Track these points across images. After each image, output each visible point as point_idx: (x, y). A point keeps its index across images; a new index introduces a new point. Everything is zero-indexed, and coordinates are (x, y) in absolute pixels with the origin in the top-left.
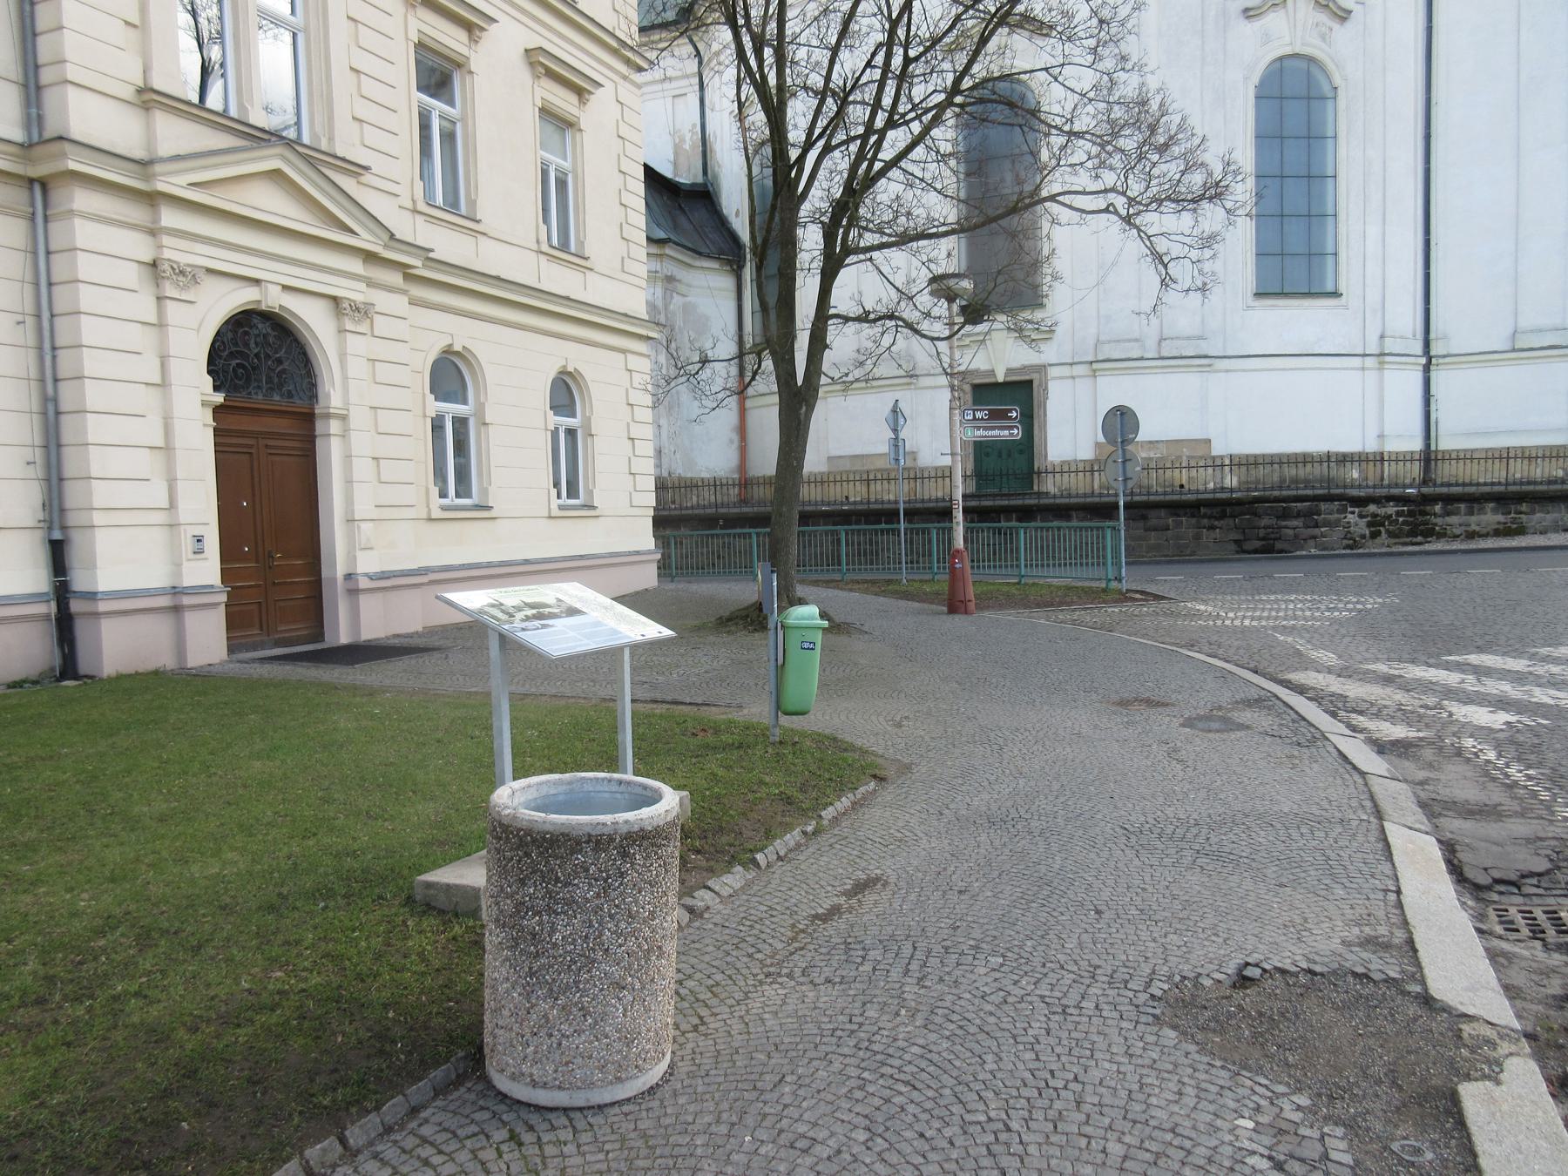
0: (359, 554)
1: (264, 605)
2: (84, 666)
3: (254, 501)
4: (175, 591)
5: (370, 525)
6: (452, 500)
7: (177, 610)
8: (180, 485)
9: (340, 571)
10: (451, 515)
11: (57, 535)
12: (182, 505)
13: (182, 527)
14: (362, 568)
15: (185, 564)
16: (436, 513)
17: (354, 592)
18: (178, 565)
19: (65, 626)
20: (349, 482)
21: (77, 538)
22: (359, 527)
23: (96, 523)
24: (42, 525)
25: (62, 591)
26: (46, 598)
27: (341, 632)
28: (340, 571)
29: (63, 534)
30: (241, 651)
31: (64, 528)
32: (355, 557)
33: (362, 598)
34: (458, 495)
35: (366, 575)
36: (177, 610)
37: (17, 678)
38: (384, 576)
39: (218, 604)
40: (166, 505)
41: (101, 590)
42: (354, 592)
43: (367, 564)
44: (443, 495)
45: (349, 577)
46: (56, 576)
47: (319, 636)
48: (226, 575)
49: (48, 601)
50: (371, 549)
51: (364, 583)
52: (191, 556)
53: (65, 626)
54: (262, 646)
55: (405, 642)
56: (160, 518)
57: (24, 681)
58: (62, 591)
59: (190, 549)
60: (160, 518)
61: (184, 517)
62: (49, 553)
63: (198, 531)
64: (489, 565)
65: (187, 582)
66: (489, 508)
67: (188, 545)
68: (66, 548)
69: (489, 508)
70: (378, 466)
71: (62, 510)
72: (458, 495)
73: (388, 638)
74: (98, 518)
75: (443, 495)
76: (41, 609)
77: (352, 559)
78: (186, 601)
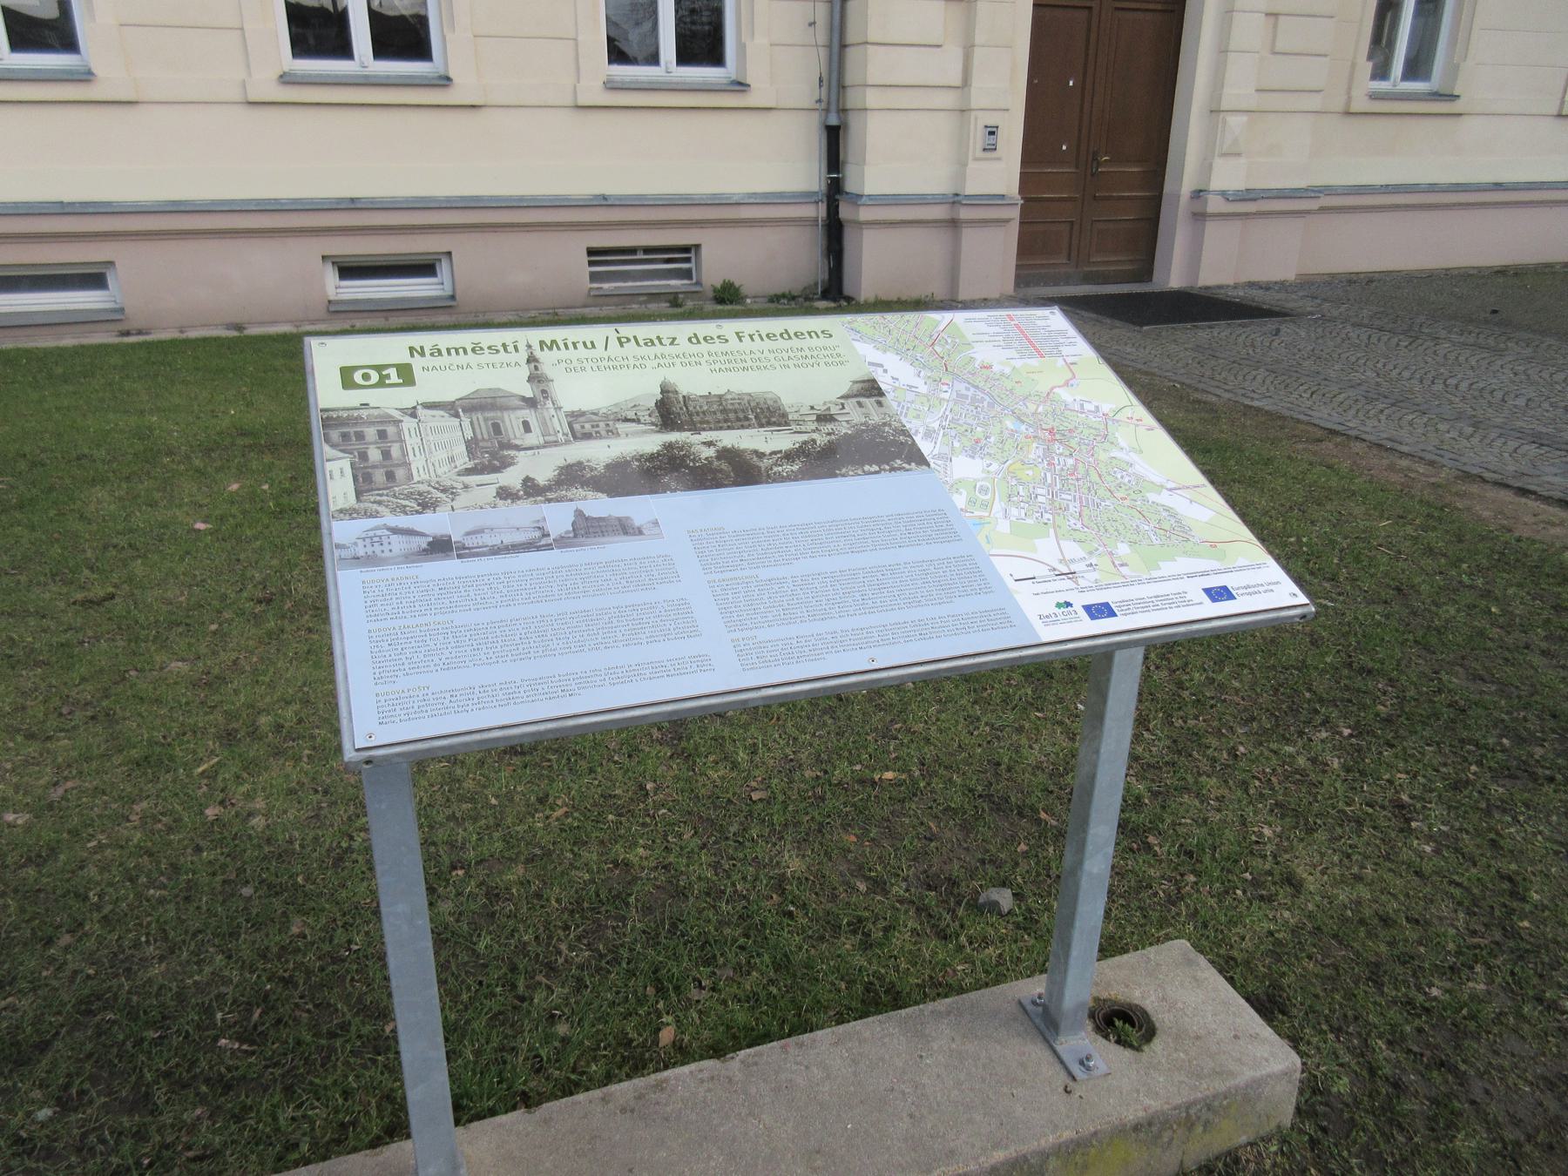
0: (1218, 163)
1: (1076, 227)
2: (848, 289)
3: (1084, 82)
4: (956, 200)
5: (1244, 118)
6: (1397, 78)
7: (954, 224)
8: (978, 53)
9: (1188, 186)
10: (1384, 109)
11: (833, 121)
12: (976, 83)
13: (973, 114)
14: (1217, 183)
15: (972, 165)
16: (1361, 104)
17: (1200, 217)
18: (962, 164)
19: (834, 233)
20: (1223, 51)
21: (854, 121)
22: (1225, 122)
23: (868, 106)
24: (817, 106)
25: (835, 190)
26: (816, 198)
27: (1173, 275)
28: (1188, 186)
29: (839, 118)
30: (1037, 284)
31: (843, 111)
32: (1211, 165)
33: (1211, 228)
34: (684, 57)
35: (1223, 193)
36: (954, 224)
37: (779, 291)
38: (1248, 196)
39: (1007, 221)
40: (957, 81)
41: (867, 192)
42: (1200, 217)
43: (1228, 177)
44: (1381, 72)
45: (1198, 194)
46: (829, 172)
47: (1146, 273)
48: (1025, 179)
49: (817, 203)
50: (1239, 155)
51: (1214, 205)
52: (980, 154)
53: (834, 233)
54: (1067, 280)
55: (1258, 296)
56: (947, 99)
57: (784, 296)
58: (835, 190)
59: (979, 146)
60: (947, 99)
61: (978, 99)
62: (824, 142)
63: (992, 120)
64: (1433, 188)
65: (971, 188)
66: (1453, 97)
67: (978, 138)
68: (841, 132)
69: (1453, 97)
70: (1275, 27)
71: (842, 87)
72: (684, 57)
73: (1235, 287)
74: (872, 98)
75: (1381, 72)
76: (809, 211)
77: (1207, 169)
78: (964, 214)
